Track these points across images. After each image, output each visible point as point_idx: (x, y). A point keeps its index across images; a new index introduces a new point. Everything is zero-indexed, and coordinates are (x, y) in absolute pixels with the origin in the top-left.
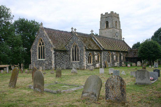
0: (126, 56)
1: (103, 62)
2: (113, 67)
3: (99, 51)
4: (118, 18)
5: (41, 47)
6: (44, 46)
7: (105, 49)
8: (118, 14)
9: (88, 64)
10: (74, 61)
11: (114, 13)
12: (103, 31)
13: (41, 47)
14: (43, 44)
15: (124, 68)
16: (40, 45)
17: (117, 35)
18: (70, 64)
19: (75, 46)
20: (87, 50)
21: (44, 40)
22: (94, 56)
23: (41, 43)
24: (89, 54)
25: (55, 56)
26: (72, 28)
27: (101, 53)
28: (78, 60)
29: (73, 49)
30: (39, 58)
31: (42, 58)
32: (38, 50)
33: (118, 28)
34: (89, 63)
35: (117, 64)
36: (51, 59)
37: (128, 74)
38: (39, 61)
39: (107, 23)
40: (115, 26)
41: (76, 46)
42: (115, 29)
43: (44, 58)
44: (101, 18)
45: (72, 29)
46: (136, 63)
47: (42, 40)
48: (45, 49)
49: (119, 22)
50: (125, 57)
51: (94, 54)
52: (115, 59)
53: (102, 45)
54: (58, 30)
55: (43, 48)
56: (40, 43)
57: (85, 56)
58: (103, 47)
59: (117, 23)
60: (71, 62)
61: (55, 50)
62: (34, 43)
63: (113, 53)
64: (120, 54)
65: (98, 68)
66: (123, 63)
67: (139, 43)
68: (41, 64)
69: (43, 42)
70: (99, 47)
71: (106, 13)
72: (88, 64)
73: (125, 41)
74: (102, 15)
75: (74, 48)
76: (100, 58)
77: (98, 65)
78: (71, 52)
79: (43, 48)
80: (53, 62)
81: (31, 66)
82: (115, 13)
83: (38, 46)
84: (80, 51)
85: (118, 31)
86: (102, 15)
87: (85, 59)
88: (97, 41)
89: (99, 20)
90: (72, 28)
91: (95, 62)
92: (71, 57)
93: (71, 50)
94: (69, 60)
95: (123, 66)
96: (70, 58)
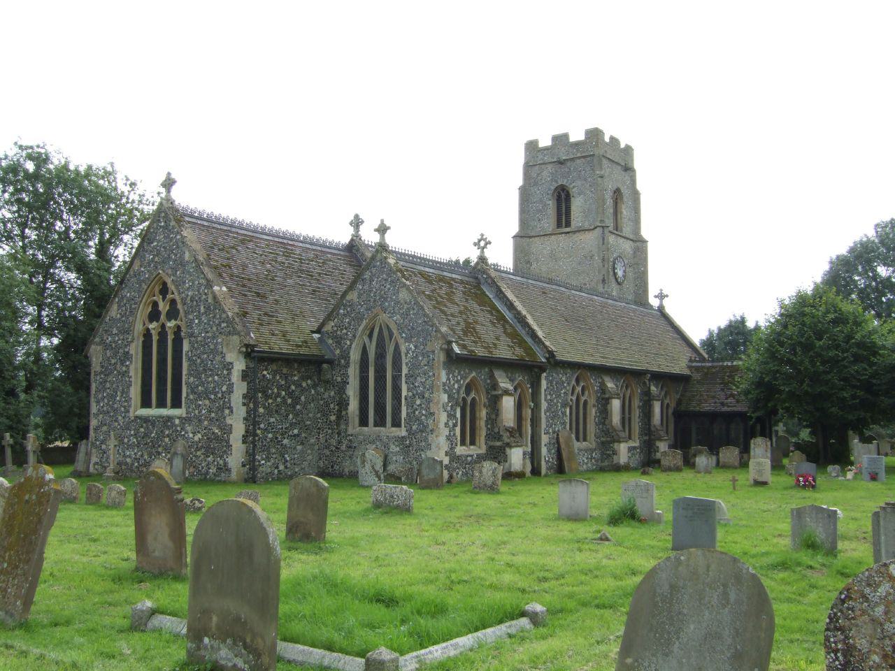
0: (679, 402)
1: (545, 439)
2: (602, 470)
3: (531, 368)
4: (628, 169)
5: (163, 333)
6: (179, 327)
7: (559, 357)
8: (628, 150)
9: (460, 450)
10: (371, 430)
11: (607, 139)
12: (542, 248)
13: (163, 333)
14: (173, 314)
15: (675, 476)
16: (154, 315)
17: (620, 273)
18: (344, 447)
19: (381, 329)
20: (453, 361)
21: (178, 284)
22: (494, 403)
23: (163, 307)
24: (464, 383)
25: (249, 397)
26: (357, 216)
27: (536, 385)
28: (396, 423)
29: (364, 352)
30: (146, 403)
31: (162, 404)
32: (135, 349)
33: (627, 230)
34: (463, 443)
35: (631, 449)
36: (227, 411)
37: (755, 508)
38: (146, 420)
39: (563, 197)
40: (610, 223)
41: (386, 333)
42: (611, 239)
43: (176, 404)
44: (528, 167)
45: (357, 223)
46: (746, 450)
47: (171, 287)
48: (186, 346)
49: (636, 196)
50: (671, 411)
51: (495, 386)
52: (616, 418)
53: (540, 334)
54: (243, 436)
55: (170, 337)
56: (155, 304)
57: (445, 397)
58: (547, 343)
59: (622, 202)
60: (350, 431)
61: (250, 353)
62: (115, 307)
63: (603, 384)
64: (647, 393)
65: (520, 475)
66: (663, 446)
67: (743, 321)
68: (154, 438)
69: (173, 302)
70: (522, 343)
71: (560, 140)
72: (460, 450)
73: (670, 310)
74: (531, 147)
75: (374, 343)
76: (527, 413)
77: (517, 457)
78: (353, 372)
79: (170, 337)
80: (238, 429)
81: (88, 454)
82: (612, 138)
83: (139, 328)
84: (414, 366)
85: (627, 247)
86: (531, 147)
87: (443, 417)
88: (511, 306)
89: (516, 179)
90: (357, 216)
91: (499, 438)
92: (353, 406)
93: (355, 356)
94: (339, 417)
95: (664, 462)
96: (343, 404)
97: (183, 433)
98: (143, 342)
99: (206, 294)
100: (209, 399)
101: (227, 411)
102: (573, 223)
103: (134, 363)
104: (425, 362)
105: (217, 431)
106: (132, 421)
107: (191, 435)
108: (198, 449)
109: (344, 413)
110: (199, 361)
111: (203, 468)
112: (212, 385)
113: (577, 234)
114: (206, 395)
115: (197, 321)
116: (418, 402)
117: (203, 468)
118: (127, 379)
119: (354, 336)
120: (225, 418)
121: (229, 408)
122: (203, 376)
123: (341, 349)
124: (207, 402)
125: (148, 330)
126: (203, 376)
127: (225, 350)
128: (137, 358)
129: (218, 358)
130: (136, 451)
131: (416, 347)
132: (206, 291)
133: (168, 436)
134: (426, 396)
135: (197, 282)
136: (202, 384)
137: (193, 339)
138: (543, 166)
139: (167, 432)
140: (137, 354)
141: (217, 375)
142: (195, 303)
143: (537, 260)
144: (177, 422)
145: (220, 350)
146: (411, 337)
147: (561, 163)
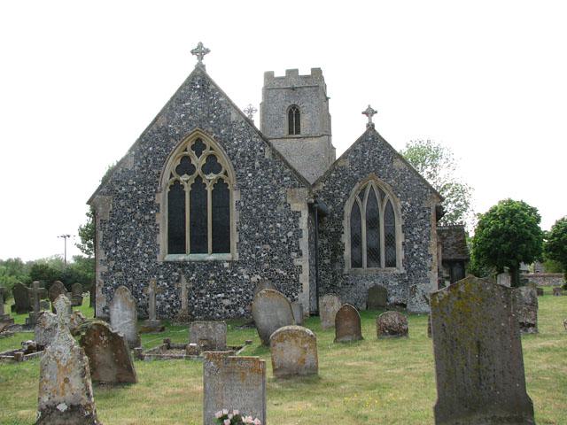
5: (198, 185)
13: (198, 185)
14: (212, 165)
16: (185, 166)
18: (340, 285)
23: (198, 162)
29: (356, 207)
30: (176, 244)
31: (199, 247)
32: (162, 199)
74: (269, 76)
83: (166, 180)
86: (269, 76)
93: (348, 210)
94: (333, 261)
96: (338, 250)
97: (235, 275)
98: (169, 193)
99: (261, 151)
101: (295, 254)
102: (302, 132)
103: (161, 211)
104: (421, 215)
105: (281, 272)
106: (161, 266)
107: (246, 277)
109: (339, 257)
110: (254, 210)
112: (274, 232)
113: (306, 139)
116: (416, 247)
118: (151, 227)
119: (348, 195)
120: (292, 260)
121: (296, 251)
122: (261, 223)
123: (334, 206)
124: (268, 247)
125: (177, 181)
126: (261, 223)
127: (289, 201)
128: (164, 207)
129: (280, 208)
130: (167, 294)
131: (412, 204)
132: (262, 148)
133: (214, 278)
137: (245, 190)
138: (279, 91)
139: (212, 275)
140: (164, 204)
142: (247, 159)
144: (226, 265)
146: (407, 197)
147: (293, 89)
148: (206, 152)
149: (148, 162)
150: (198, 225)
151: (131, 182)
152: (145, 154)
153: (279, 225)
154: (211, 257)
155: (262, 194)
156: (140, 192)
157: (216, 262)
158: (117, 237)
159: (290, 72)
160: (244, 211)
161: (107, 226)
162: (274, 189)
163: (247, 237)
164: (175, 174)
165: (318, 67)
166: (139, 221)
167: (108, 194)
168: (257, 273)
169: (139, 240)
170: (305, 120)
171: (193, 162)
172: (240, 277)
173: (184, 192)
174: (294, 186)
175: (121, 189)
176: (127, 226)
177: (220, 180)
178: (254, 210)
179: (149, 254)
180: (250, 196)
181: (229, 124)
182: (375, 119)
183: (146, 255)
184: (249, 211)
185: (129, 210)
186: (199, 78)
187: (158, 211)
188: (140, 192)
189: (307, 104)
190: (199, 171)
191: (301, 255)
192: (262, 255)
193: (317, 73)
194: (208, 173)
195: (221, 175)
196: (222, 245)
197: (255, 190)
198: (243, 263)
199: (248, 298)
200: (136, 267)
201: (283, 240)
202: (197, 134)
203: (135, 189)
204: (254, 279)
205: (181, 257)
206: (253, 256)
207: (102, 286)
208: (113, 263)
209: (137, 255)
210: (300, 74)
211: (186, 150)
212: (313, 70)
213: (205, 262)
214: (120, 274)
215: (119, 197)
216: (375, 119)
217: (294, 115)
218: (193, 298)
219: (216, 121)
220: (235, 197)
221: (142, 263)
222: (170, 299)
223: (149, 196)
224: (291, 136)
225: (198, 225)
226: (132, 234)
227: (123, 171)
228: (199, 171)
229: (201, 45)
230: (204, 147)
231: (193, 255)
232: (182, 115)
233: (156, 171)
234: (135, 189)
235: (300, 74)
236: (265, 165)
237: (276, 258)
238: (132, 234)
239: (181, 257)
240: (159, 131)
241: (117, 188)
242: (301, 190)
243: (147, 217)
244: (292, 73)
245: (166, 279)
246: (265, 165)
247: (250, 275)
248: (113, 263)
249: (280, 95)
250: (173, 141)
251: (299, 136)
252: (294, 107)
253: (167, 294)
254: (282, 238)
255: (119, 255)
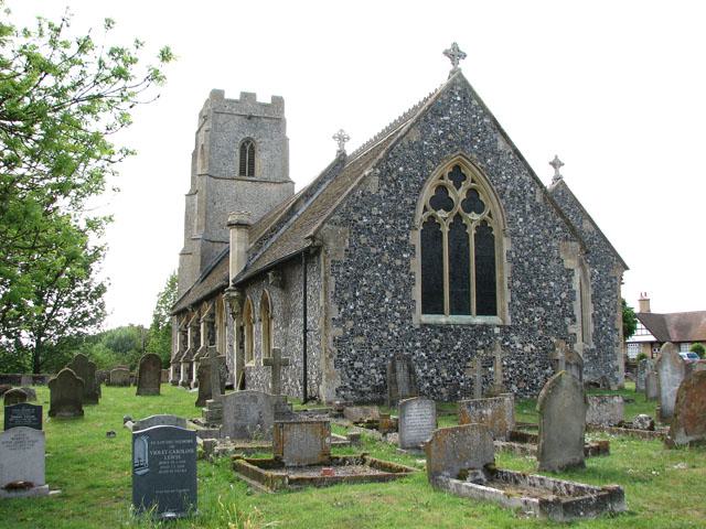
5: (458, 225)
13: (458, 225)
14: (474, 202)
16: (441, 200)
30: (432, 303)
31: (460, 307)
74: (217, 95)
83: (420, 217)
86: (217, 95)
97: (507, 343)
100: (544, 306)
101: (568, 320)
104: (609, 285)
106: (417, 330)
107: (519, 346)
108: (530, 361)
111: (538, 382)
114: (540, 301)
115: (521, 220)
116: (604, 319)
117: (538, 382)
120: (566, 327)
121: (570, 316)
122: (534, 280)
124: (541, 309)
125: (432, 218)
127: (562, 256)
129: (554, 263)
130: (426, 367)
132: (532, 189)
134: (611, 314)
135: (518, 177)
136: (533, 289)
139: (480, 343)
141: (554, 280)
142: (516, 199)
143: (222, 201)
144: (497, 330)
145: (556, 254)
147: (250, 117)
148: (466, 185)
149: (398, 187)
150: (459, 278)
151: (375, 211)
152: (394, 176)
153: (552, 284)
154: (480, 320)
155: (533, 246)
156: (388, 227)
157: (486, 327)
158: (356, 285)
159: (245, 95)
160: (517, 264)
161: (342, 270)
162: (547, 240)
163: (519, 297)
164: (429, 206)
165: (253, 92)
166: (389, 266)
167: (343, 224)
168: (530, 342)
169: (387, 293)
170: (261, 160)
171: (451, 195)
172: (512, 346)
173: (467, 235)
174: (566, 239)
175: (361, 219)
176: (370, 273)
177: (484, 222)
178: (527, 263)
179: (402, 313)
180: (521, 246)
181: (497, 154)
182: (562, 171)
183: (397, 314)
184: (521, 264)
185: (373, 250)
186: (459, 88)
187: (413, 255)
188: (388, 227)
189: (267, 140)
190: (458, 207)
191: (575, 320)
192: (536, 319)
193: (278, 102)
194: (469, 212)
195: (485, 215)
196: (487, 306)
197: (526, 239)
198: (514, 329)
199: (521, 372)
200: (383, 330)
201: (362, 303)
202: (459, 159)
203: (381, 221)
204: (527, 349)
205: (442, 319)
206: (526, 320)
207: (335, 357)
208: (351, 323)
209: (385, 314)
210: (226, 97)
211: (442, 178)
212: (274, 98)
213: (472, 326)
214: (360, 340)
215: (358, 230)
216: (562, 171)
217: (248, 153)
218: (458, 374)
219: (481, 146)
220: (505, 246)
221: (392, 325)
222: (429, 375)
223: (400, 234)
224: (243, 177)
225: (459, 278)
226: (377, 283)
227: (363, 195)
228: (458, 207)
229: (455, 47)
230: (464, 177)
231: (428, 316)
232: (441, 132)
233: (410, 201)
234: (381, 221)
235: (226, 97)
236: (536, 209)
237: (550, 323)
238: (377, 283)
239: (442, 319)
240: (411, 148)
241: (356, 218)
242: (574, 244)
243: (398, 262)
244: (248, 97)
245: (424, 348)
246: (536, 209)
247: (524, 344)
248: (351, 323)
249: (232, 122)
250: (429, 163)
251: (254, 179)
252: (248, 140)
253: (426, 367)
254: (556, 299)
255: (359, 313)
